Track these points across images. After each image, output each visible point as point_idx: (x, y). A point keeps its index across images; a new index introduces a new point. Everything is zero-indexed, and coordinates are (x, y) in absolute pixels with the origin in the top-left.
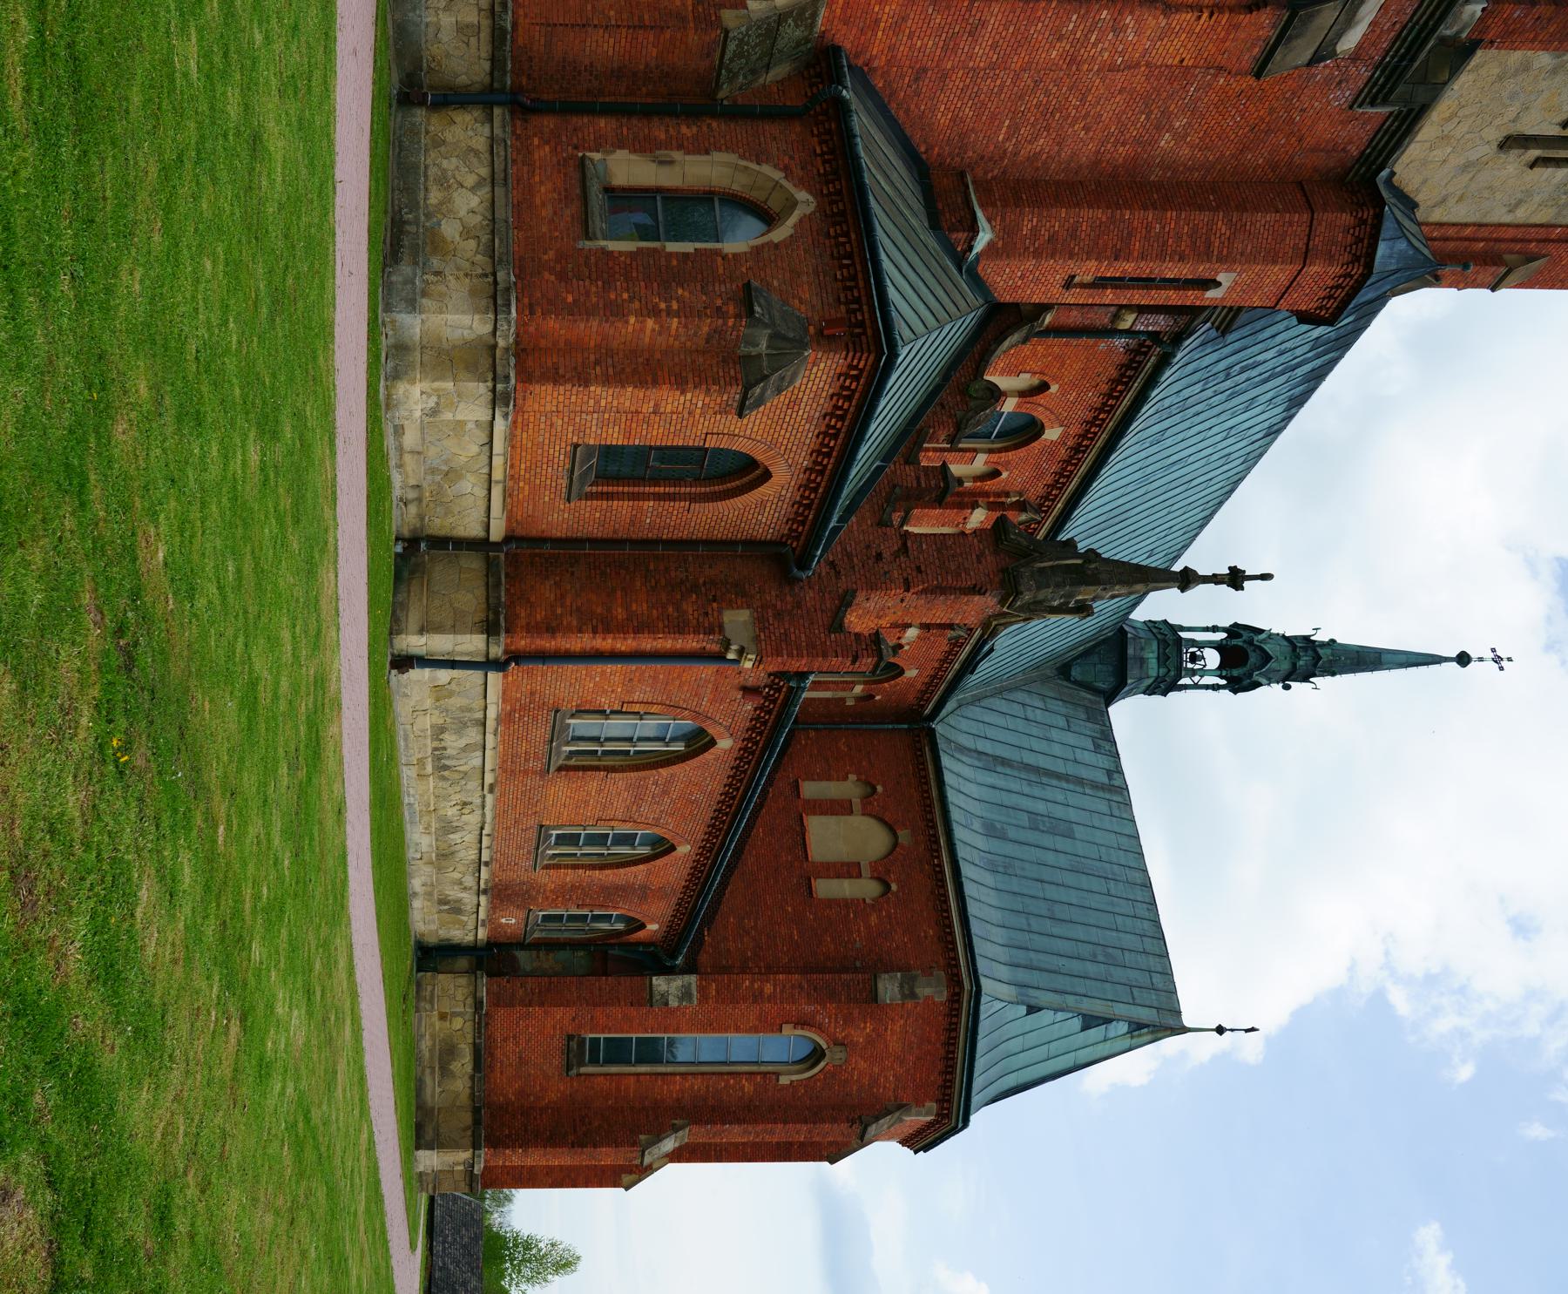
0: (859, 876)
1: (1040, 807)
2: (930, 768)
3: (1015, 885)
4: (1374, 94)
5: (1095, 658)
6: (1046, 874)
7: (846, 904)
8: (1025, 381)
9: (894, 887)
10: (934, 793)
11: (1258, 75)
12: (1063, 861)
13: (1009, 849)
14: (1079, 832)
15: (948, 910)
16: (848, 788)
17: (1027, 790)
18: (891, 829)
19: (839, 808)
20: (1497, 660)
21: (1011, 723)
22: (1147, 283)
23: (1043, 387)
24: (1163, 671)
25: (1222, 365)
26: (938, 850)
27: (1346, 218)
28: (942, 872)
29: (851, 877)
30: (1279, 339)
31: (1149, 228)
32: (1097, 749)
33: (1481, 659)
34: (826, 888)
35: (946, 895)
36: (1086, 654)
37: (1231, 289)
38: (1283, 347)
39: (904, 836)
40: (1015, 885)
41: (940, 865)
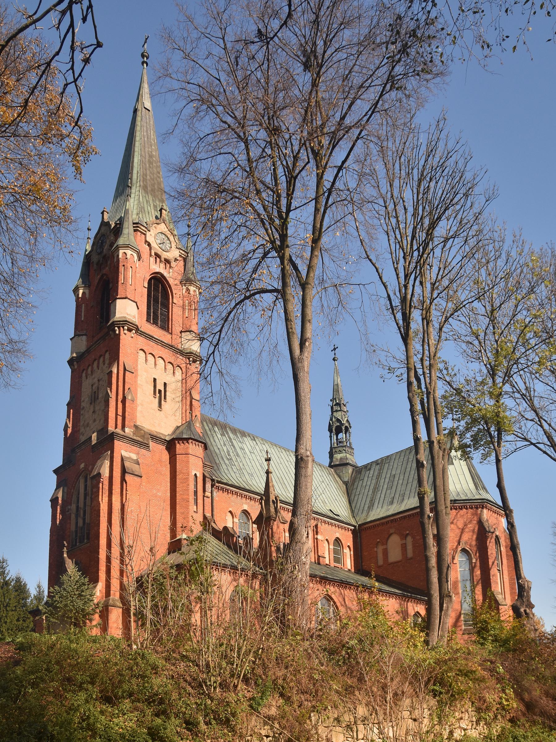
0: (405, 544)
1: (385, 486)
2: (375, 523)
3: (407, 493)
4: (146, 446)
5: (341, 474)
6: (405, 482)
7: (414, 546)
8: (229, 516)
9: (408, 532)
10: (378, 522)
11: (141, 477)
12: (402, 477)
13: (397, 496)
14: (393, 473)
15: (413, 514)
16: (380, 550)
17: (380, 492)
18: (390, 535)
19: (385, 553)
20: (335, 349)
21: (360, 499)
22: (196, 493)
23: (230, 512)
24: (344, 452)
25: (227, 462)
26: (395, 519)
27: (178, 446)
28: (401, 517)
29: (406, 546)
30: (219, 447)
31: (181, 494)
32: (370, 469)
33: (335, 354)
34: (410, 554)
35: (408, 515)
36: (340, 477)
37: (197, 470)
38: (222, 445)
39: (392, 531)
40: (407, 493)
41: (400, 518)
